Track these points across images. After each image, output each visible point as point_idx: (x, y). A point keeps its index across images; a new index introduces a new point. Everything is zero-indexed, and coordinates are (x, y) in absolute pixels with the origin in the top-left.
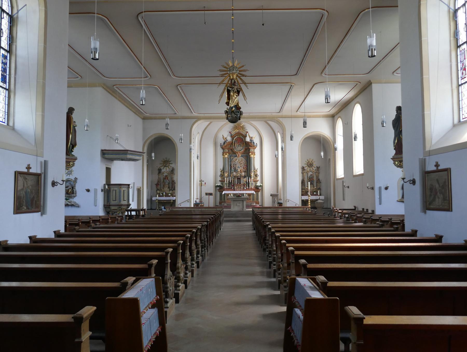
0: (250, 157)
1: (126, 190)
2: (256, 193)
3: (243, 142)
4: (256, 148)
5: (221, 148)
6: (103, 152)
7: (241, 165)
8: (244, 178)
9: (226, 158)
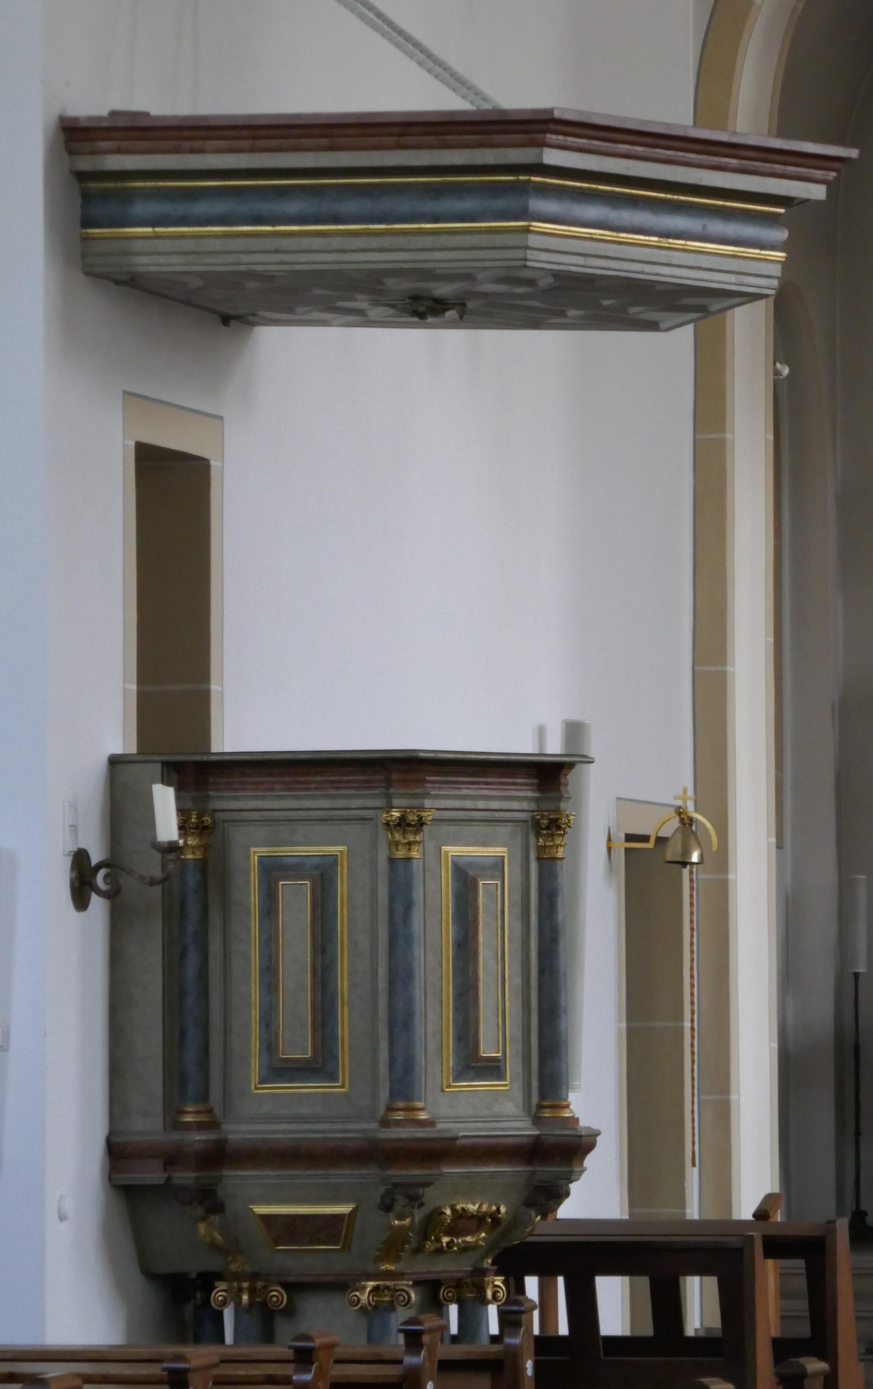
1: (498, 865)
6: (85, 164)
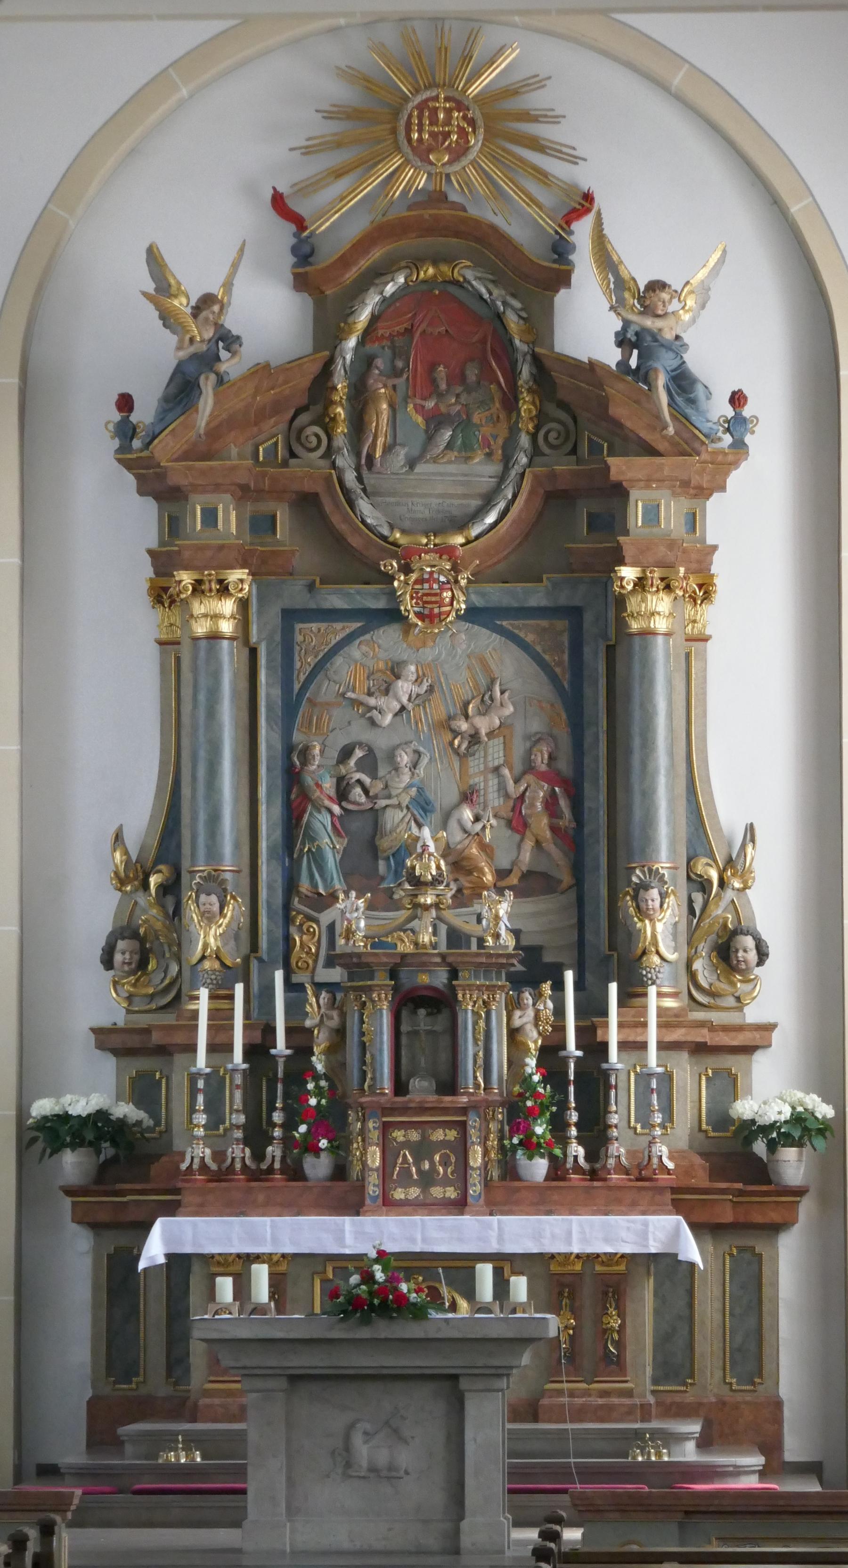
0: (621, 624)
2: (731, 1243)
3: (512, 375)
4: (734, 479)
5: (130, 479)
7: (475, 765)
8: (518, 982)
9: (213, 655)
